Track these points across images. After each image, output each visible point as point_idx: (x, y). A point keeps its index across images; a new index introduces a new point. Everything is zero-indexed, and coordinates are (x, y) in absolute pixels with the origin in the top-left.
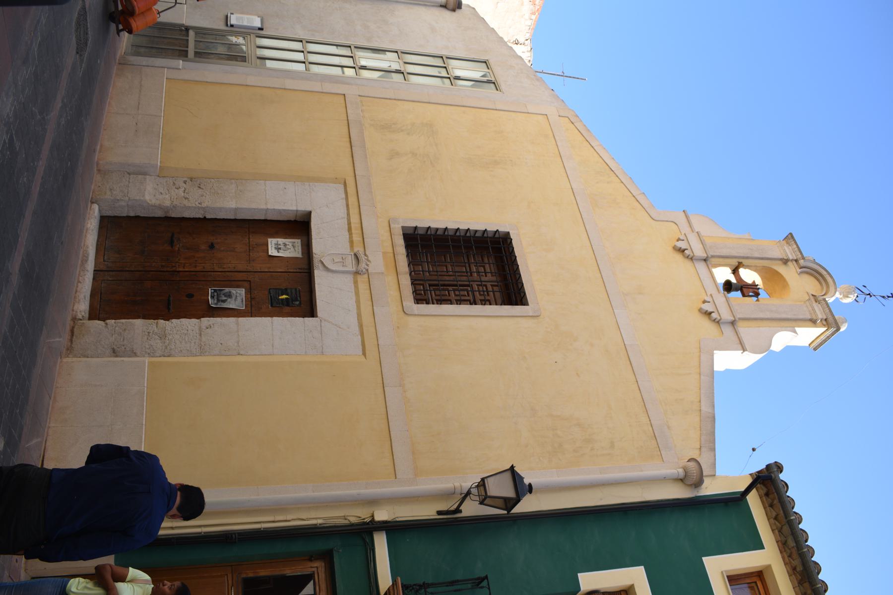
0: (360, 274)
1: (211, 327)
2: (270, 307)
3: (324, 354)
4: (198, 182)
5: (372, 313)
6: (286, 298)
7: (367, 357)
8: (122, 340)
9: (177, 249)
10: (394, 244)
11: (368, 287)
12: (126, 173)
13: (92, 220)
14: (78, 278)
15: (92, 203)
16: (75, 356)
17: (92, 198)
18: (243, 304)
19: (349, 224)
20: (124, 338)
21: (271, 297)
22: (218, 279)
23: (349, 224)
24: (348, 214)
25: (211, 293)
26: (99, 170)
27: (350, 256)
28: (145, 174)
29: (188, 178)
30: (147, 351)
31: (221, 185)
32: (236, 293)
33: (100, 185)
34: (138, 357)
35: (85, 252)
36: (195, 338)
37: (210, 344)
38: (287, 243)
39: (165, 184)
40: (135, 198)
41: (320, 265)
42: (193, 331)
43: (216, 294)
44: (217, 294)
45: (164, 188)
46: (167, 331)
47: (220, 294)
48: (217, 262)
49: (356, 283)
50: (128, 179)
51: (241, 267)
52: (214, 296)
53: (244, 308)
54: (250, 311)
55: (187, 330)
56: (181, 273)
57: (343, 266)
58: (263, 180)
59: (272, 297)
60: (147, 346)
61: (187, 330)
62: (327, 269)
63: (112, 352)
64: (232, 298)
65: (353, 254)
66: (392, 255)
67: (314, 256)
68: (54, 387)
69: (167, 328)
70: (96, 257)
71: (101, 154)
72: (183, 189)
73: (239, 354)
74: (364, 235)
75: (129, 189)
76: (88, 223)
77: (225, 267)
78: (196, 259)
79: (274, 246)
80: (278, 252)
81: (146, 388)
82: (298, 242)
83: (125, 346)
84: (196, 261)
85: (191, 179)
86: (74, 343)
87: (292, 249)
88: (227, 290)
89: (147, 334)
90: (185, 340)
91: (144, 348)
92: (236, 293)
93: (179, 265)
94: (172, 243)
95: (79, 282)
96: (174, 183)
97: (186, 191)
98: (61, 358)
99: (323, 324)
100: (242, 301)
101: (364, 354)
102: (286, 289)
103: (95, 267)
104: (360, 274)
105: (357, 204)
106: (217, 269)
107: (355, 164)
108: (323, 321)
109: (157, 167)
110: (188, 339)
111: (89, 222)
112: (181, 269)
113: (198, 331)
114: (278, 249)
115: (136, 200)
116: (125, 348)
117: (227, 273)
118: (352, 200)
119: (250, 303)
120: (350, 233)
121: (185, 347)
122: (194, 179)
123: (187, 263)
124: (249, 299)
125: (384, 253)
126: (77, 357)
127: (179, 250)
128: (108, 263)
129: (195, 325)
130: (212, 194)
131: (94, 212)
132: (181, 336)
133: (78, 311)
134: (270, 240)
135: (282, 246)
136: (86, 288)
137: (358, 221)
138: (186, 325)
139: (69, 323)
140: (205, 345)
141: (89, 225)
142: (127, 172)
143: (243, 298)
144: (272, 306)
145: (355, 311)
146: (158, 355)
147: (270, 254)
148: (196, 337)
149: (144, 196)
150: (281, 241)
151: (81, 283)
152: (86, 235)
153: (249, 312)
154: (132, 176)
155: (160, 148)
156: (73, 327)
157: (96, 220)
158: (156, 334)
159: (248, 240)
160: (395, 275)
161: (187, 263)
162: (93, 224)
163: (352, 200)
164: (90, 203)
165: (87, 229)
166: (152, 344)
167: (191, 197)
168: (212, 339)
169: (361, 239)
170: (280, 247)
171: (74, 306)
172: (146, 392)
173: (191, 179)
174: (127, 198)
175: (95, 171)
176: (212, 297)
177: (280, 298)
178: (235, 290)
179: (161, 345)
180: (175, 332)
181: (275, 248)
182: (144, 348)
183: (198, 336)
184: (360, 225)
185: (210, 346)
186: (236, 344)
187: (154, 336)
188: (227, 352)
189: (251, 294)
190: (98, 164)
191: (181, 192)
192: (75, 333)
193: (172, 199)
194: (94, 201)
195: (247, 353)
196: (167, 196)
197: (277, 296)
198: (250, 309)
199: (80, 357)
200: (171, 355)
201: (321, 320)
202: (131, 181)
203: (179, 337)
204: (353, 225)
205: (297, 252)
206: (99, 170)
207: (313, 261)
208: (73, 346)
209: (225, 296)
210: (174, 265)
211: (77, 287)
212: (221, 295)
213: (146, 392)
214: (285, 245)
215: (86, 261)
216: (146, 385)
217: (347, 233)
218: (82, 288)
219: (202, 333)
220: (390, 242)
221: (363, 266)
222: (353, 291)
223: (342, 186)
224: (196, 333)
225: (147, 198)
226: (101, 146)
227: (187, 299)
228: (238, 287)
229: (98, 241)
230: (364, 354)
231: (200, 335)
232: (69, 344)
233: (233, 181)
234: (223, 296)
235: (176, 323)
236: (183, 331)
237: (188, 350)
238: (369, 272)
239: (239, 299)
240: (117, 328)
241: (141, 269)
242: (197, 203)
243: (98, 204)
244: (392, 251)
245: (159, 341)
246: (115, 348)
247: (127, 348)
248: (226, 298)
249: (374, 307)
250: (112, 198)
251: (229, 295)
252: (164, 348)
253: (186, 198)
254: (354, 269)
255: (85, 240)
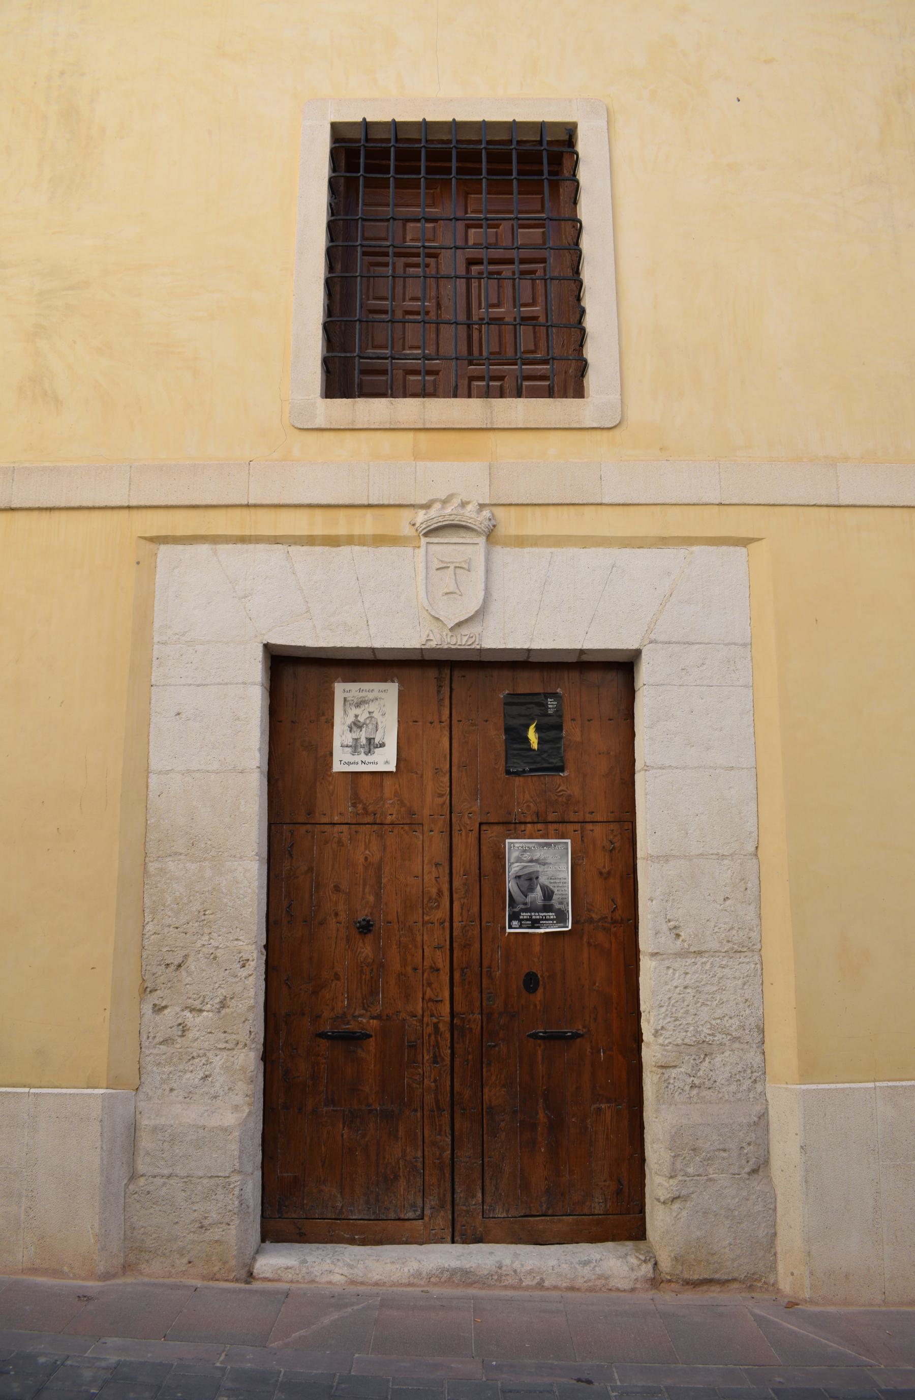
0: (494, 526)
1: (675, 927)
2: (566, 774)
3: (749, 640)
4: (160, 970)
5: (905, 510)
6: (538, 729)
7: (143, 541)
8: (725, 1154)
9: (374, 1023)
10: (388, 426)
11: (538, 510)
12: (131, 1187)
13: (317, 1270)
14: (528, 1288)
15: (250, 1276)
16: (773, 1268)
17: (237, 1280)
18: (556, 844)
19: (310, 540)
20: (719, 1150)
21: (532, 770)
22: (476, 909)
23: (310, 540)
24: (276, 540)
25: (520, 927)
26: (127, 1268)
27: (433, 548)
28: (133, 1129)
29: (142, 1001)
30: (745, 1087)
31: (169, 900)
32: (519, 860)
33: (185, 1261)
34: (767, 1109)
35: (433, 1280)
36: (708, 966)
37: (728, 927)
38: (350, 719)
39: (167, 1069)
40: (236, 1153)
41: (465, 631)
42: (686, 973)
43: (524, 915)
44: (526, 911)
45: (185, 1072)
46: (687, 1041)
47: (525, 904)
48: (421, 911)
49: (521, 541)
50: (159, 1181)
51: (437, 847)
52: (530, 919)
53: (569, 841)
54: (578, 826)
55: (685, 988)
56: (458, 1008)
57: (469, 571)
58: (148, 777)
59: (533, 767)
60: (733, 1088)
61: (685, 988)
62: (480, 614)
63: (756, 1176)
64: (538, 872)
65: (424, 540)
66: (422, 436)
67: (432, 645)
68: (883, 1309)
69: (679, 1041)
70: (406, 1243)
71: (66, 1269)
72: (187, 1014)
73: (756, 855)
74: (357, 502)
75: (201, 1173)
76: (330, 1283)
77: (434, 891)
78: (409, 969)
79: (362, 757)
80: (382, 745)
81: (878, 1084)
82: (342, 690)
83: (744, 1145)
84: (415, 969)
85: (145, 991)
86: (736, 1275)
87: (372, 707)
88: (511, 885)
89: (695, 1092)
90: (714, 992)
91: (739, 1096)
92: (519, 860)
93: (432, 1015)
94: (355, 1038)
95: (540, 1286)
96: (164, 1042)
97: (197, 1004)
98: (797, 1304)
99: (662, 638)
100: (548, 845)
101: (744, 542)
102: (508, 730)
103: (441, 1241)
104: (494, 526)
105: (237, 513)
106: (441, 913)
107: (84, 504)
108: (653, 636)
109: (112, 1095)
110: (712, 984)
111: (325, 1279)
112: (445, 1009)
113: (689, 961)
114: (371, 745)
115: (241, 1152)
116: (749, 1144)
117: (455, 884)
118: (220, 523)
119: (552, 827)
120: (350, 540)
121: (735, 991)
122: (148, 984)
123: (424, 994)
124: (539, 826)
125: (417, 456)
126: (775, 1261)
127: (378, 1017)
128: (427, 1207)
129: (668, 968)
130: (206, 931)
131: (287, 1268)
132: (703, 1004)
133: (633, 1276)
134: (337, 767)
135: (363, 735)
136: (553, 1262)
137: (302, 516)
138: (669, 991)
139: (668, 1298)
140: (728, 941)
141: (337, 1278)
142: (127, 1186)
143: (539, 844)
144: (561, 769)
145: (616, 552)
146: (759, 1058)
147: (393, 768)
148: (704, 963)
149: (226, 1130)
150: (341, 735)
151: (542, 1280)
152: (376, 1284)
153: (583, 830)
154: (141, 1168)
155: (33, 1090)
156: (687, 1282)
157: (505, 1264)
158: (697, 1068)
159: (336, 829)
160: (491, 435)
161: (424, 994)
162: (327, 1265)
163: (220, 523)
164: (256, 1285)
165: (353, 1282)
166: (727, 1075)
167: (221, 991)
168: (712, 924)
169: (369, 513)
170: (363, 741)
171: (618, 1290)
172: (890, 1084)
173: (145, 991)
174: (235, 1178)
175: (129, 1280)
176: (535, 924)
177: (535, 746)
178: (510, 866)
179: (727, 1053)
180: (690, 1019)
181: (369, 752)
182: (739, 1096)
183: (704, 960)
184: (318, 512)
185: (732, 928)
186: (726, 862)
187: (701, 1073)
188: (749, 885)
189: (525, 823)
190: (107, 1276)
191: (198, 1020)
192: (706, 1276)
193: (228, 1046)
194: (243, 1273)
195: (751, 833)
196: (218, 1061)
197: (531, 753)
198: (571, 827)
199: (775, 1254)
200: (757, 1027)
201: (651, 642)
202: (166, 1172)
203: (705, 1009)
204: (318, 531)
205: (382, 695)
206: (127, 1268)
207: (449, 650)
208: (743, 1276)
209: (531, 889)
210: (430, 1029)
211: (556, 1288)
212: (528, 900)
213: (890, 1084)
214: (356, 725)
215: (466, 1272)
216: (871, 1085)
217: (345, 550)
218: (559, 1275)
219: (692, 949)
220: (378, 435)
221: (470, 515)
222: (549, 550)
223: (164, 550)
224: (695, 963)
225: (230, 1119)
226: (34, 1271)
227: (540, 990)
228: (500, 857)
229: (352, 1242)
230: (744, 542)
231: (700, 953)
232: (736, 1285)
233: (153, 867)
234: (531, 896)
235: (664, 1018)
236: (689, 998)
237: (744, 984)
238: (487, 502)
239: (539, 854)
240: (690, 1170)
241: (446, 1115)
242: (243, 973)
243: (254, 1259)
244: (411, 435)
245: (719, 1058)
246: (747, 1169)
247: (748, 1139)
248: (539, 888)
249: (605, 501)
250: (237, 1222)
251: (529, 880)
252: (736, 1045)
253: (223, 1004)
254: (482, 540)
255: (394, 1284)
